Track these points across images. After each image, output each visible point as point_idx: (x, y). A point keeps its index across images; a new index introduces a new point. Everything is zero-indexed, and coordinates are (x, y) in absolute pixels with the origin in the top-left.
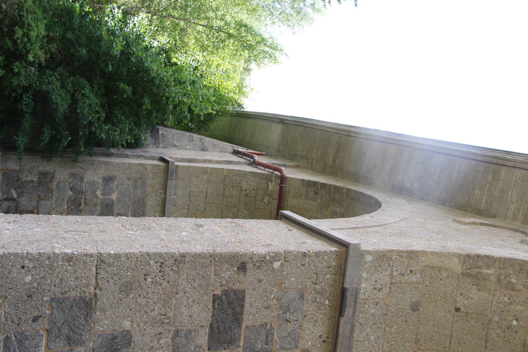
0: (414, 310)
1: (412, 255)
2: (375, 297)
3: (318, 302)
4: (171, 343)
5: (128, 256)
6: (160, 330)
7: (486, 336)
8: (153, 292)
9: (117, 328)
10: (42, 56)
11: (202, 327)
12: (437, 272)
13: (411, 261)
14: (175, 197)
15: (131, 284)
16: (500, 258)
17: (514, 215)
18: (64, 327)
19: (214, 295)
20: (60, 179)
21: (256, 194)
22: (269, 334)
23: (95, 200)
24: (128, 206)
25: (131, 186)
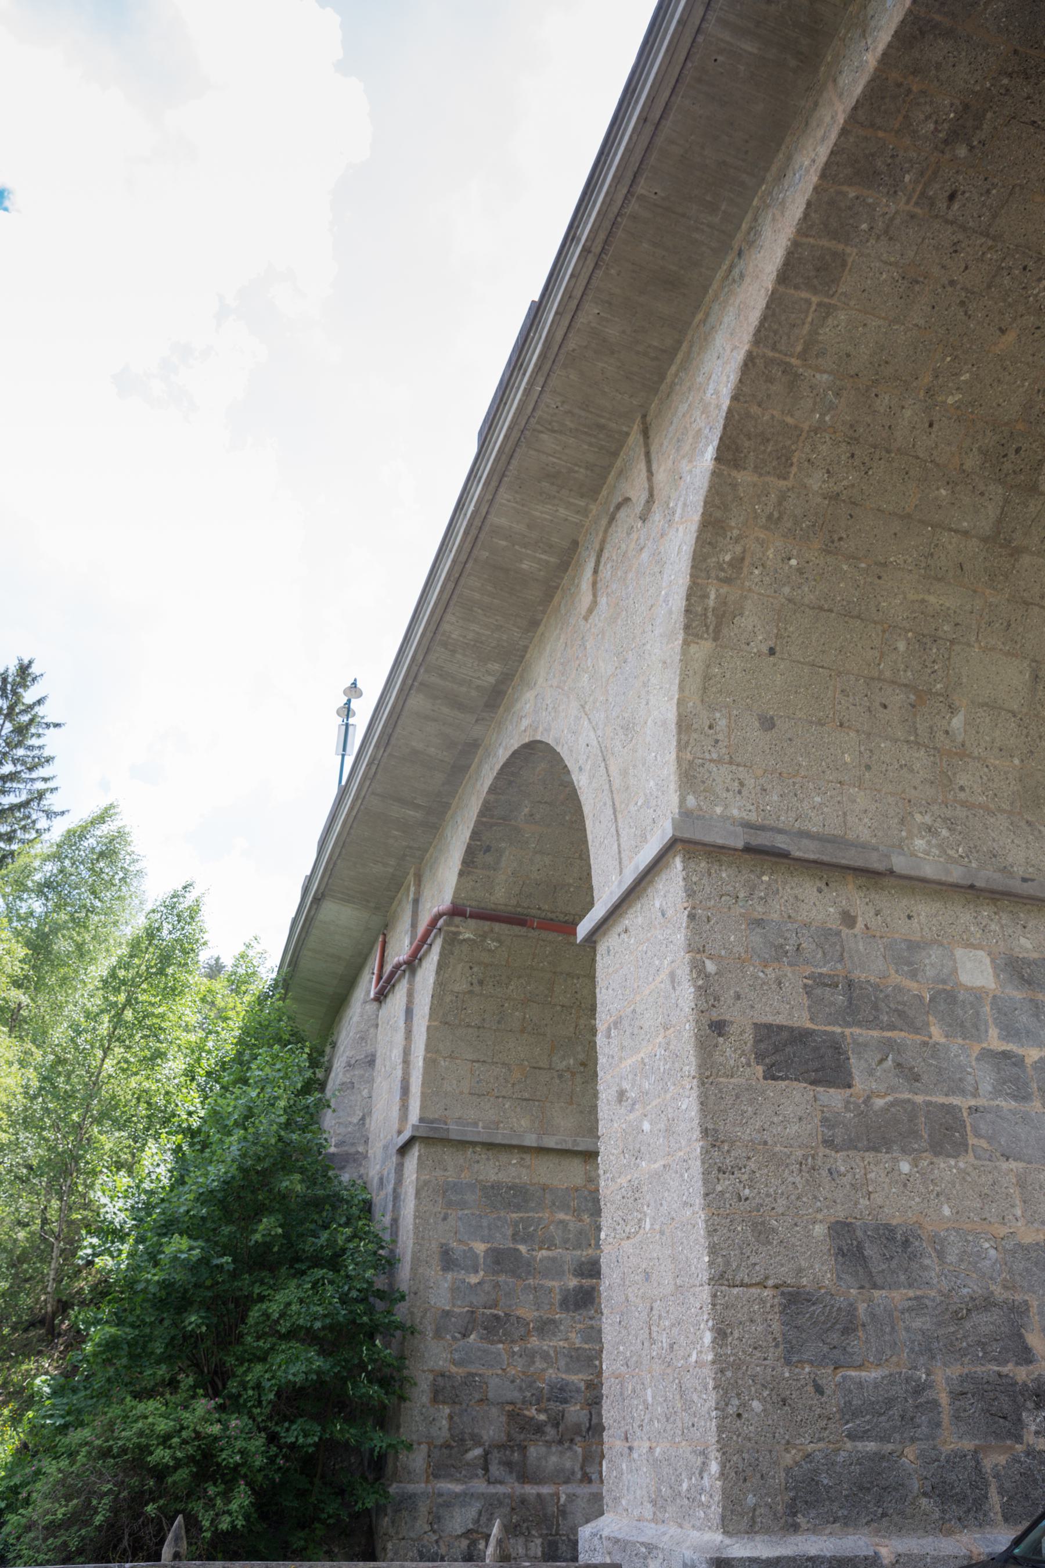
0: (773, 726)
1: (684, 724)
2: (753, 791)
3: (767, 895)
4: (844, 1153)
5: (711, 1232)
6: (825, 1173)
7: (813, 608)
8: (766, 1186)
9: (825, 1248)
10: (203, 1405)
11: (816, 1099)
12: (711, 682)
13: (695, 726)
14: (481, 1124)
15: (755, 1225)
16: (691, 576)
17: (578, 512)
18: (828, 1341)
19: (765, 1078)
20: (445, 1360)
21: (479, 964)
22: (821, 981)
23: (487, 1287)
24: (499, 1218)
25: (460, 1213)
